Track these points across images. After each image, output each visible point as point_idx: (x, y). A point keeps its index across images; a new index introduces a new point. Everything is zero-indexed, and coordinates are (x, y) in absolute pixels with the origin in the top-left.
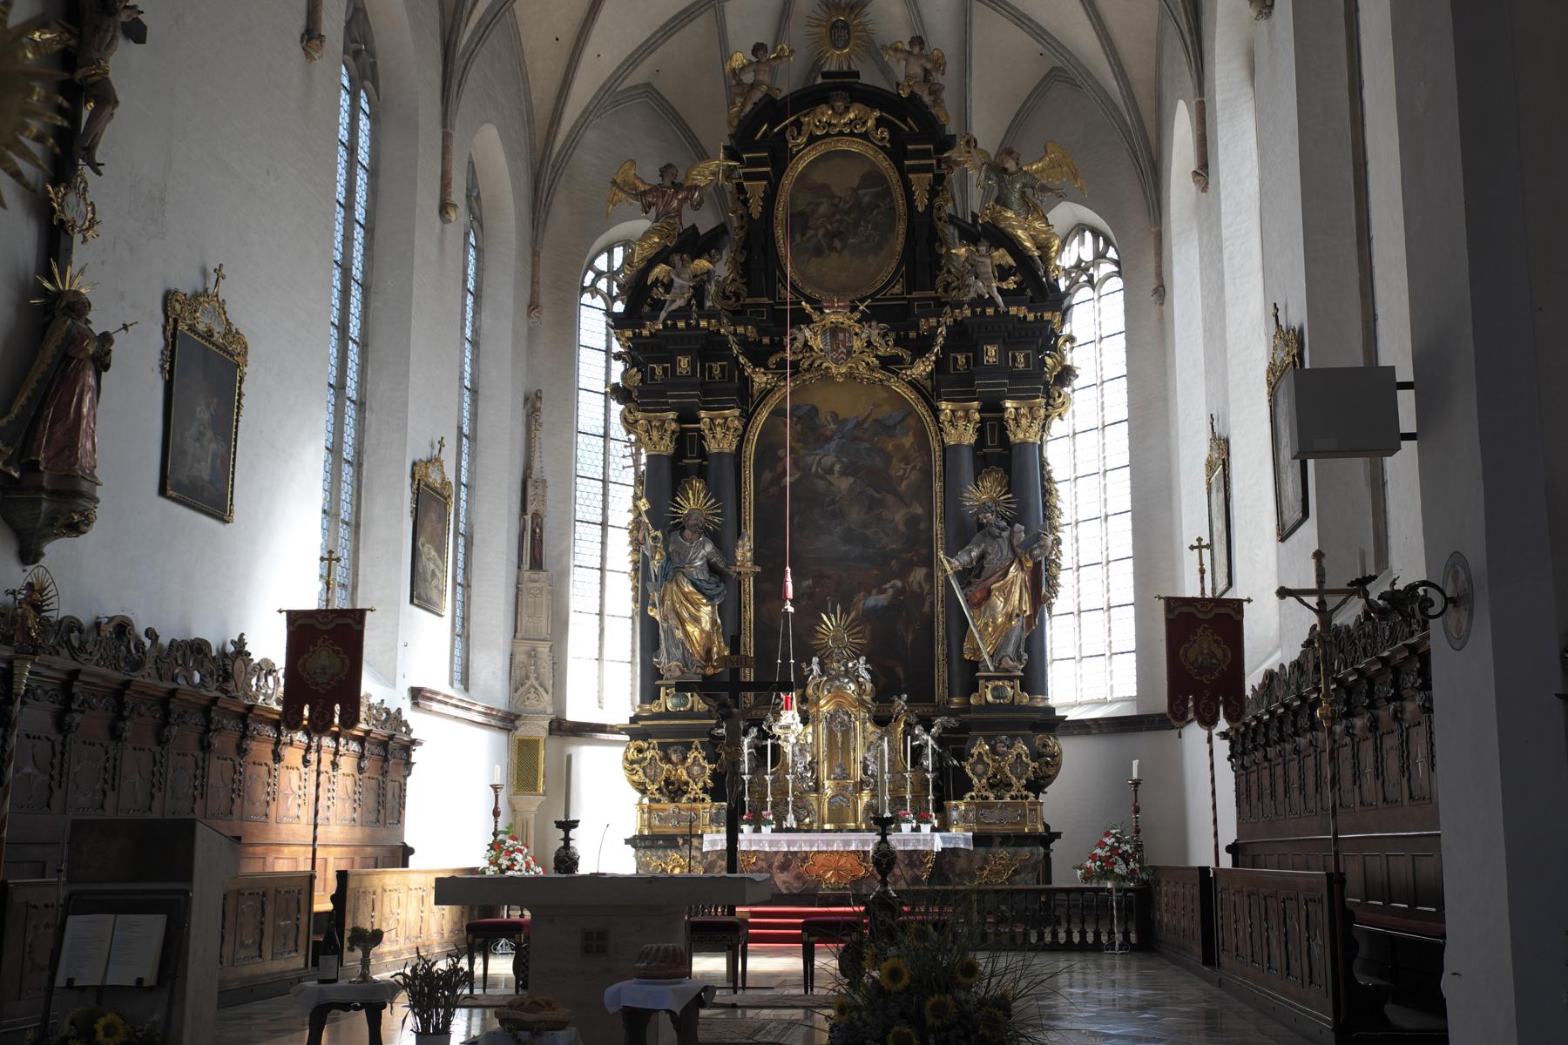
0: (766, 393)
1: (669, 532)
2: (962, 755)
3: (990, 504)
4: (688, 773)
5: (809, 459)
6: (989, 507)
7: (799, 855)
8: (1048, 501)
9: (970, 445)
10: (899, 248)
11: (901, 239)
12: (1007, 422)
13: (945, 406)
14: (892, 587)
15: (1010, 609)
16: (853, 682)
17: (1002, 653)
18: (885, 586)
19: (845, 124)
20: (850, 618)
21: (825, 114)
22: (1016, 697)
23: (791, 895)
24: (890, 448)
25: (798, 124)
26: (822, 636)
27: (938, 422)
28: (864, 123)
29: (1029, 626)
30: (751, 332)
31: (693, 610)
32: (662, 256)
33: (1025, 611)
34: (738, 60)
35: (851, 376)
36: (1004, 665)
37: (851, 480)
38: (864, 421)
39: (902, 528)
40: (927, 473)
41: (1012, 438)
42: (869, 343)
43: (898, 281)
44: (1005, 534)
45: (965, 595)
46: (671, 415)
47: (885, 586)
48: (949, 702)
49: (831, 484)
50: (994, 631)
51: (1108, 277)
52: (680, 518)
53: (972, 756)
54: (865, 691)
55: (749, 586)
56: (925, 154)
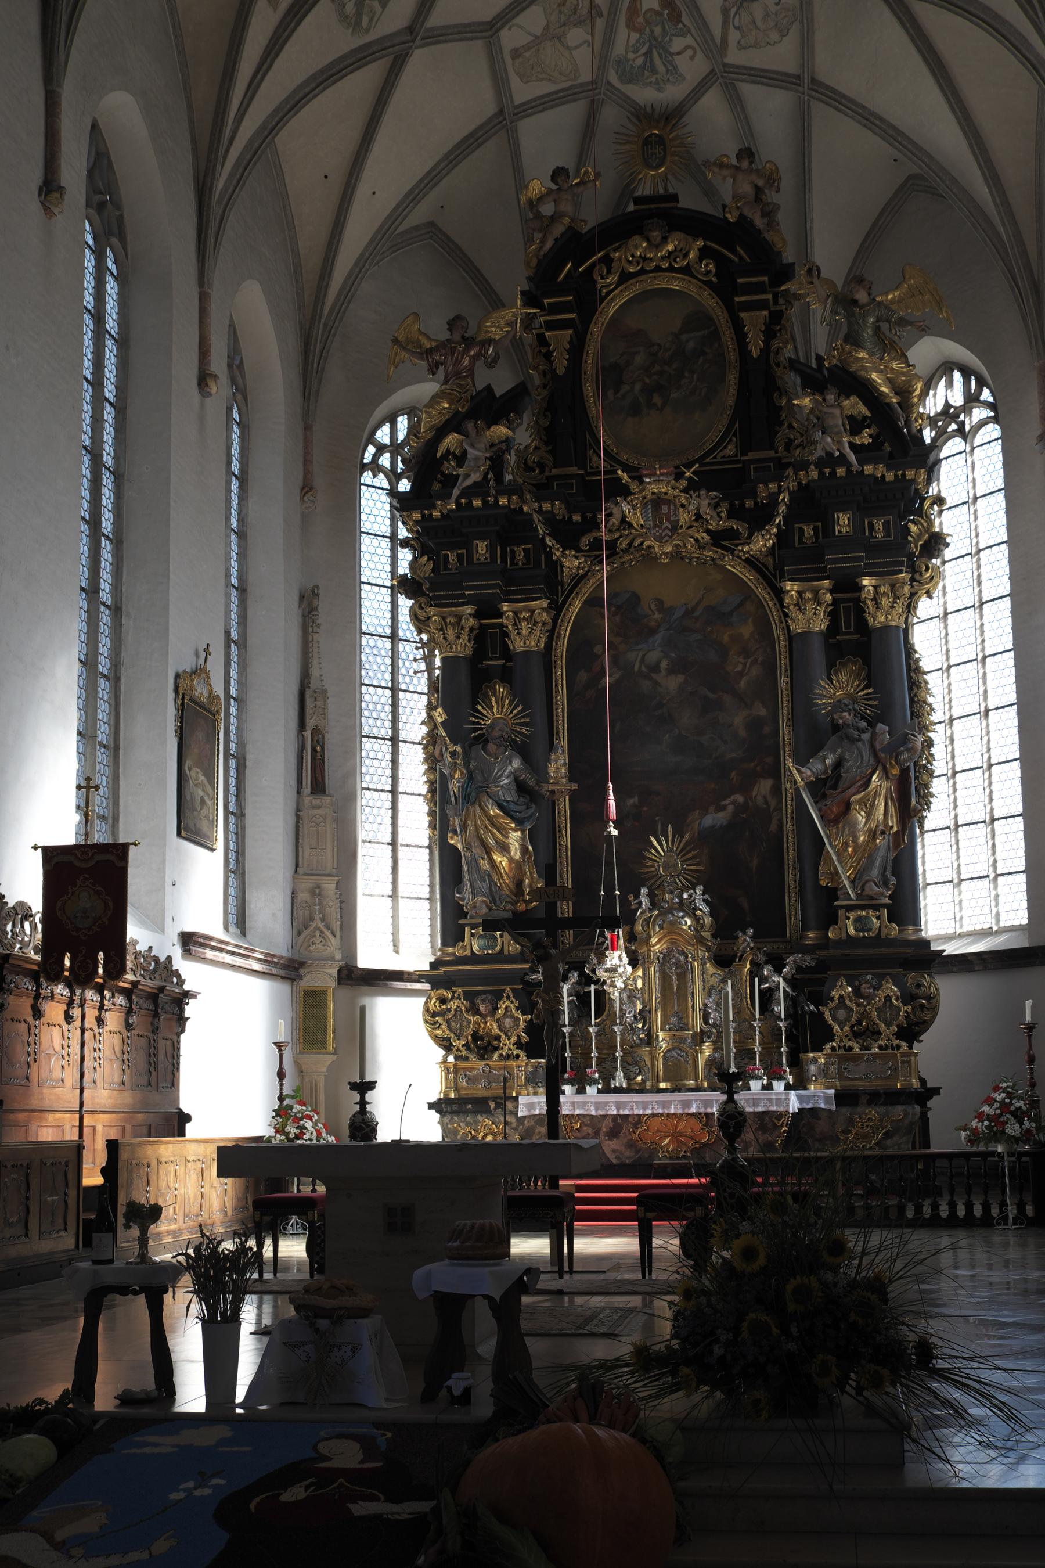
0: (579, 580)
1: (470, 746)
2: (820, 999)
3: (846, 701)
4: (499, 1026)
5: (631, 656)
6: (846, 705)
7: (630, 1119)
8: (916, 696)
9: (821, 632)
10: (731, 401)
11: (733, 391)
12: (864, 602)
13: (788, 586)
14: (733, 803)
15: (873, 825)
16: (689, 916)
17: (865, 878)
18: (723, 803)
19: (663, 258)
20: (684, 841)
21: (640, 247)
22: (883, 929)
23: (622, 1165)
24: (726, 638)
25: (607, 261)
26: (651, 863)
27: (782, 606)
28: (686, 255)
29: (897, 844)
30: (559, 508)
31: (500, 836)
32: (452, 424)
33: (892, 827)
34: (536, 188)
35: (677, 556)
36: (868, 891)
37: (681, 678)
38: (694, 609)
39: (742, 733)
40: (771, 668)
41: (871, 621)
42: (698, 516)
43: (731, 440)
44: (866, 737)
45: (820, 810)
46: (469, 610)
47: (723, 803)
48: (803, 937)
49: (656, 683)
50: (855, 851)
51: (983, 423)
52: (482, 729)
53: (832, 1000)
54: (703, 925)
55: (564, 806)
56: (759, 288)
